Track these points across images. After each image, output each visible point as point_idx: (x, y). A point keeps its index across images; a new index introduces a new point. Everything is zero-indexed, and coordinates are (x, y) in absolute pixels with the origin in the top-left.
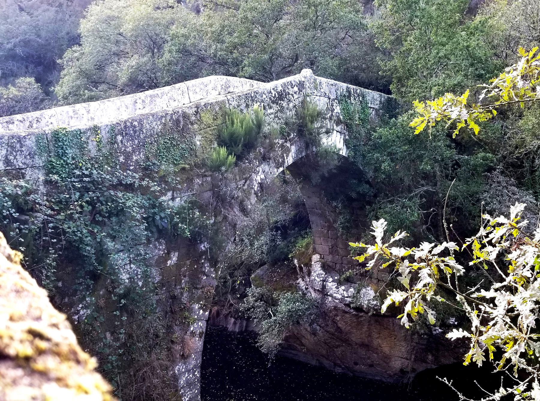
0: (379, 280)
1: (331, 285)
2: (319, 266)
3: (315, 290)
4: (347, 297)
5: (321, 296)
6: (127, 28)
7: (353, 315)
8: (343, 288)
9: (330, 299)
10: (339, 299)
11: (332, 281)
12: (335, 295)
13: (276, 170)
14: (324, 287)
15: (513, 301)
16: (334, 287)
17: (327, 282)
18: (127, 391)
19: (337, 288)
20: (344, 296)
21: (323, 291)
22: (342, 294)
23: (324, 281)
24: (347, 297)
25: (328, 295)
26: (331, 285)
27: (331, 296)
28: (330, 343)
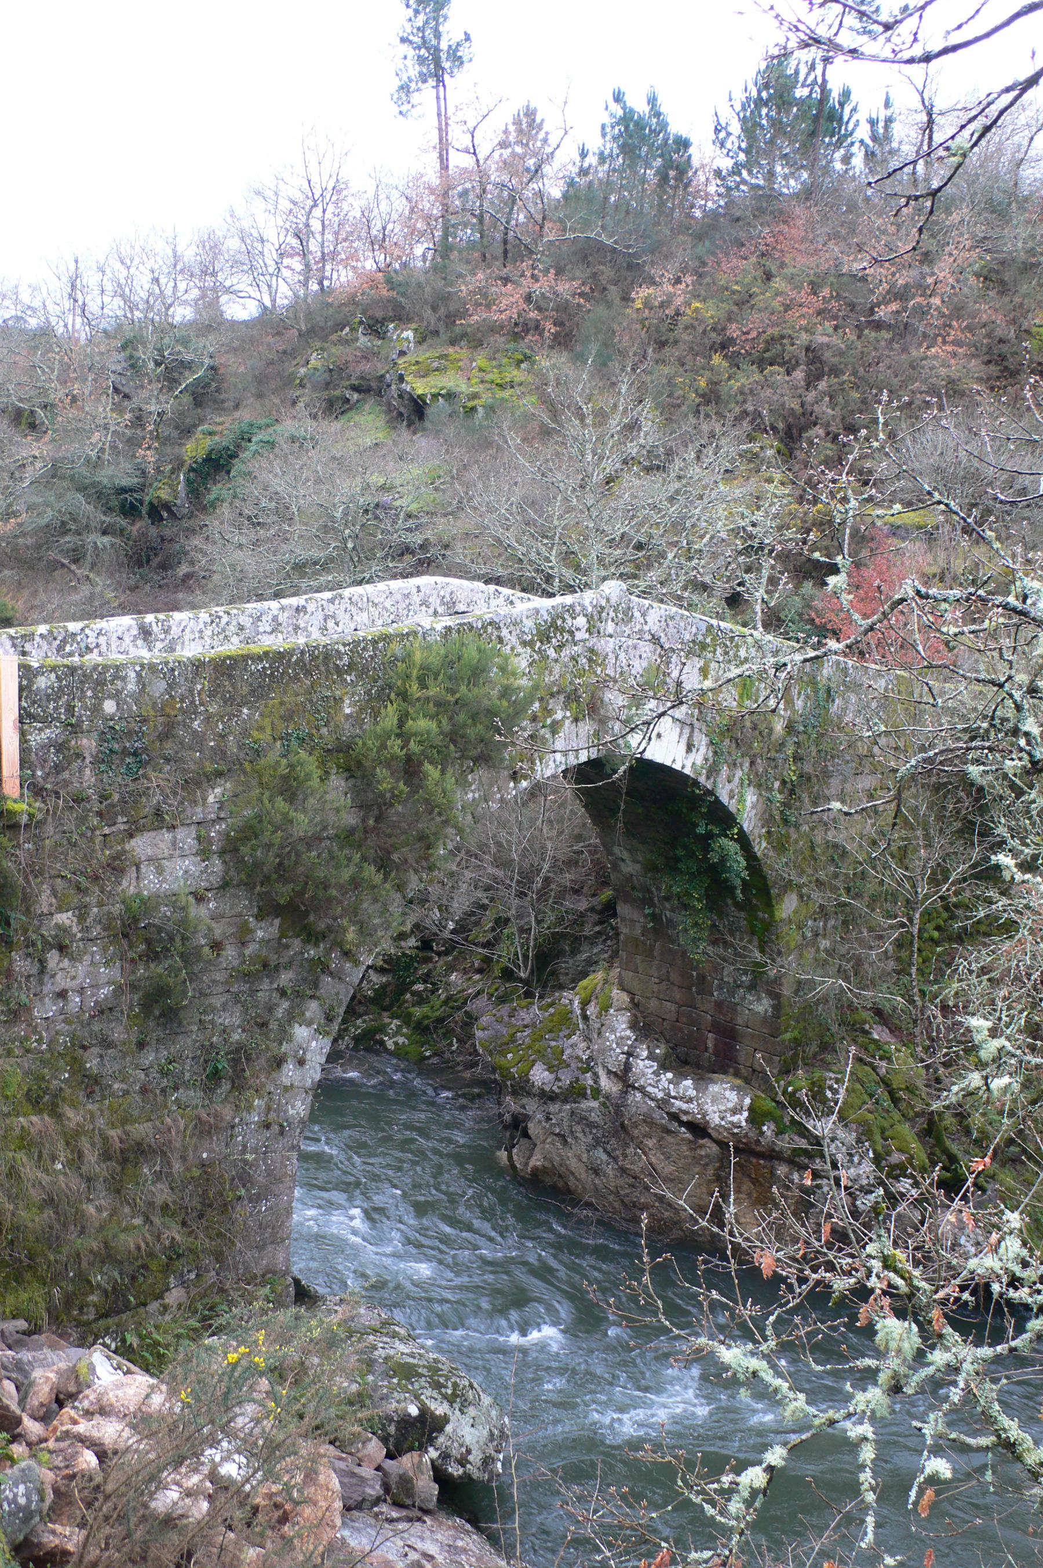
0: (754, 1071)
1: (644, 1067)
2: (625, 1019)
3: (609, 1072)
4: (675, 1098)
5: (620, 1086)
6: (200, 460)
7: (683, 1139)
8: (670, 1075)
9: (639, 1095)
10: (657, 1101)
11: (648, 1058)
12: (649, 1089)
13: (512, 784)
14: (627, 1067)
15: (618, 98)
16: (650, 1071)
17: (637, 1057)
18: (692, 1093)
19: (656, 1073)
20: (668, 1095)
21: (623, 1075)
22: (664, 1090)
23: (629, 1054)
24: (675, 1098)
25: (634, 1088)
26: (644, 1067)
27: (642, 1089)
28: (627, 1195)
